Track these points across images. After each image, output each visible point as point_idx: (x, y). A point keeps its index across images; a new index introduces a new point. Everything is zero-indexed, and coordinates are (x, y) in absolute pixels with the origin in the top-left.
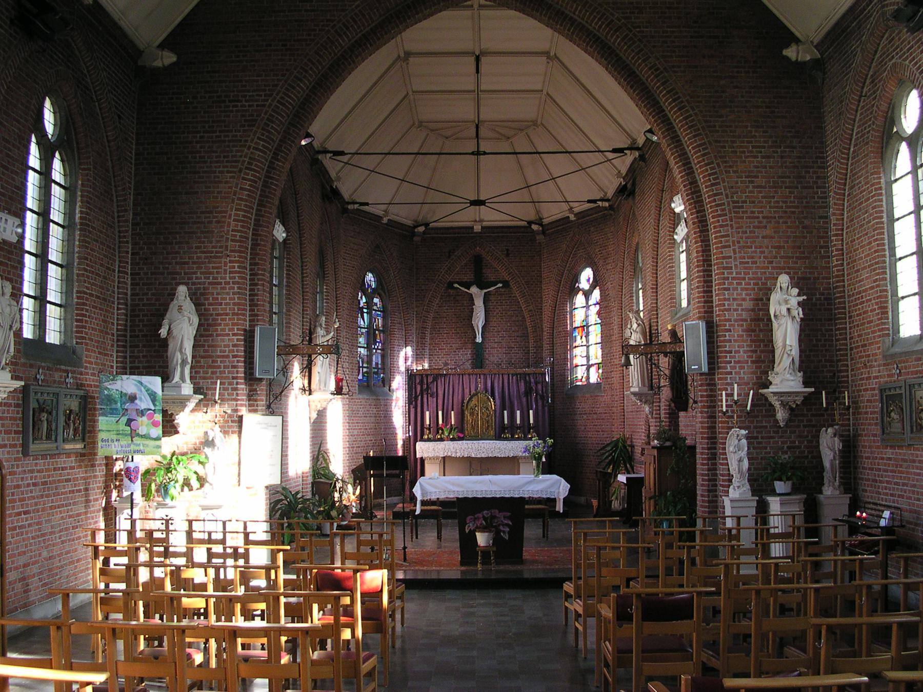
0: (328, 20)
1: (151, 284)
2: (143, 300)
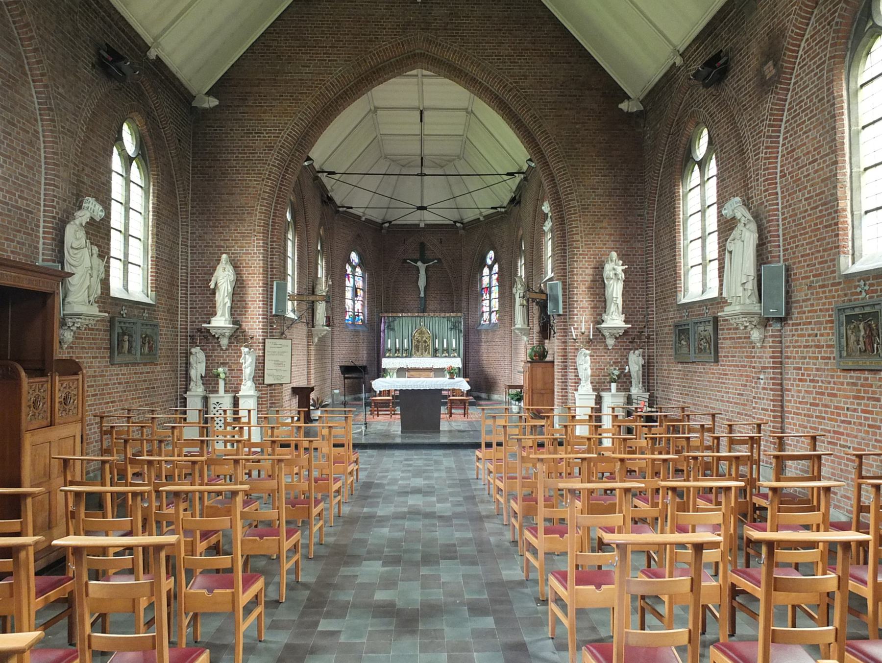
0: (320, 80)
1: (204, 253)
2: (198, 263)
